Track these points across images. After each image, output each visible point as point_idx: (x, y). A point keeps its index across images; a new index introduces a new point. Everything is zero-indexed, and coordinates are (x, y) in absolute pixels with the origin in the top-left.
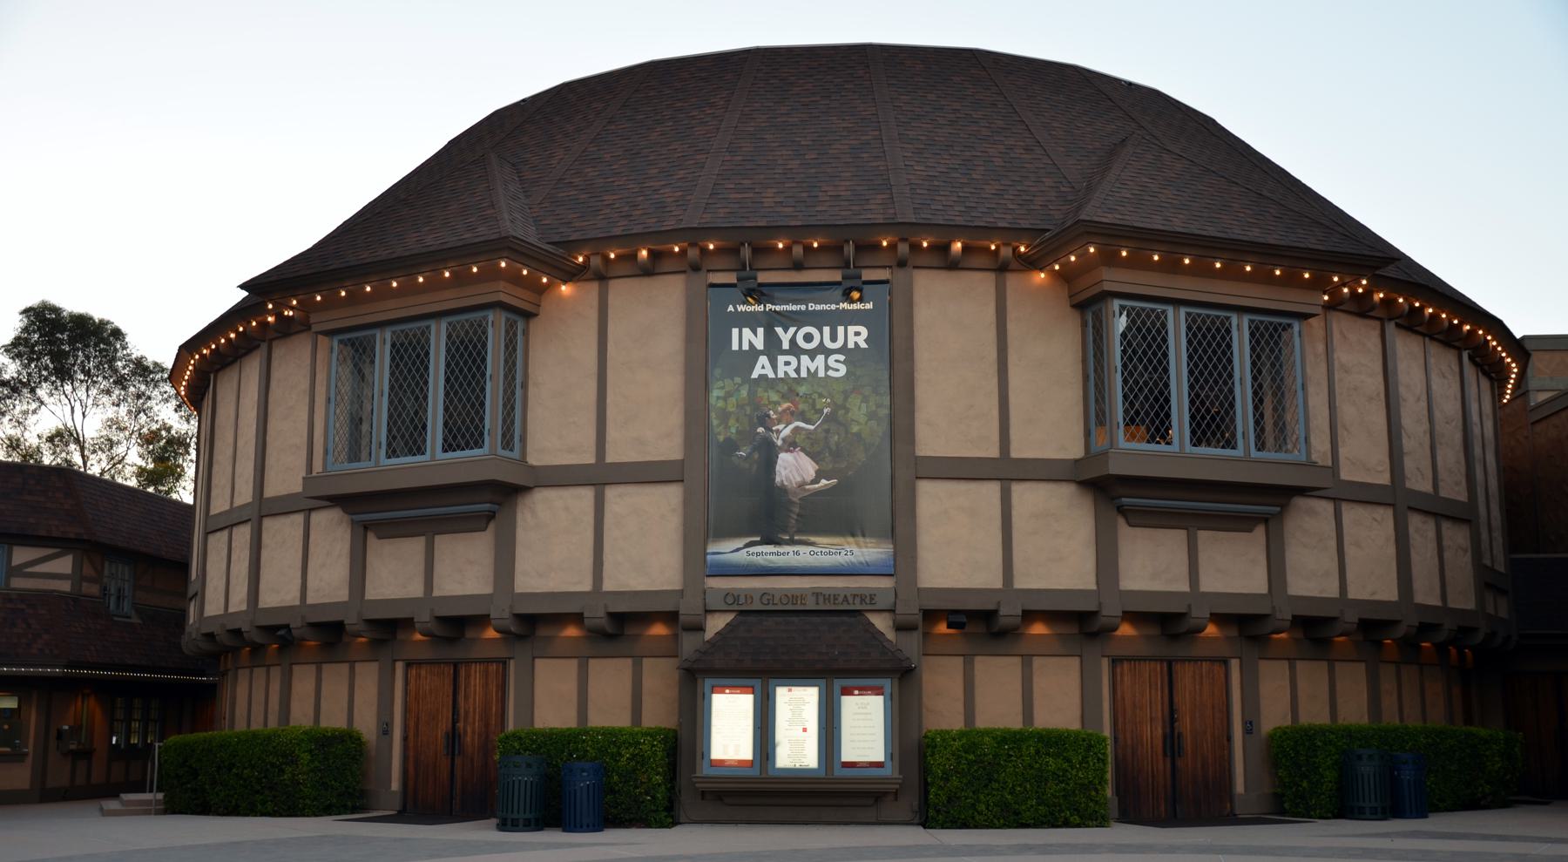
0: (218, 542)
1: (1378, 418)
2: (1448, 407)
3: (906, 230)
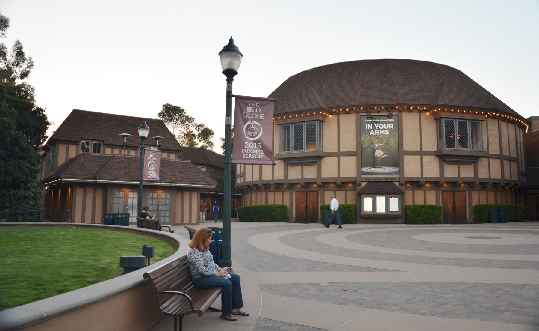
1: (497, 140)
2: (513, 137)
3: (401, 105)
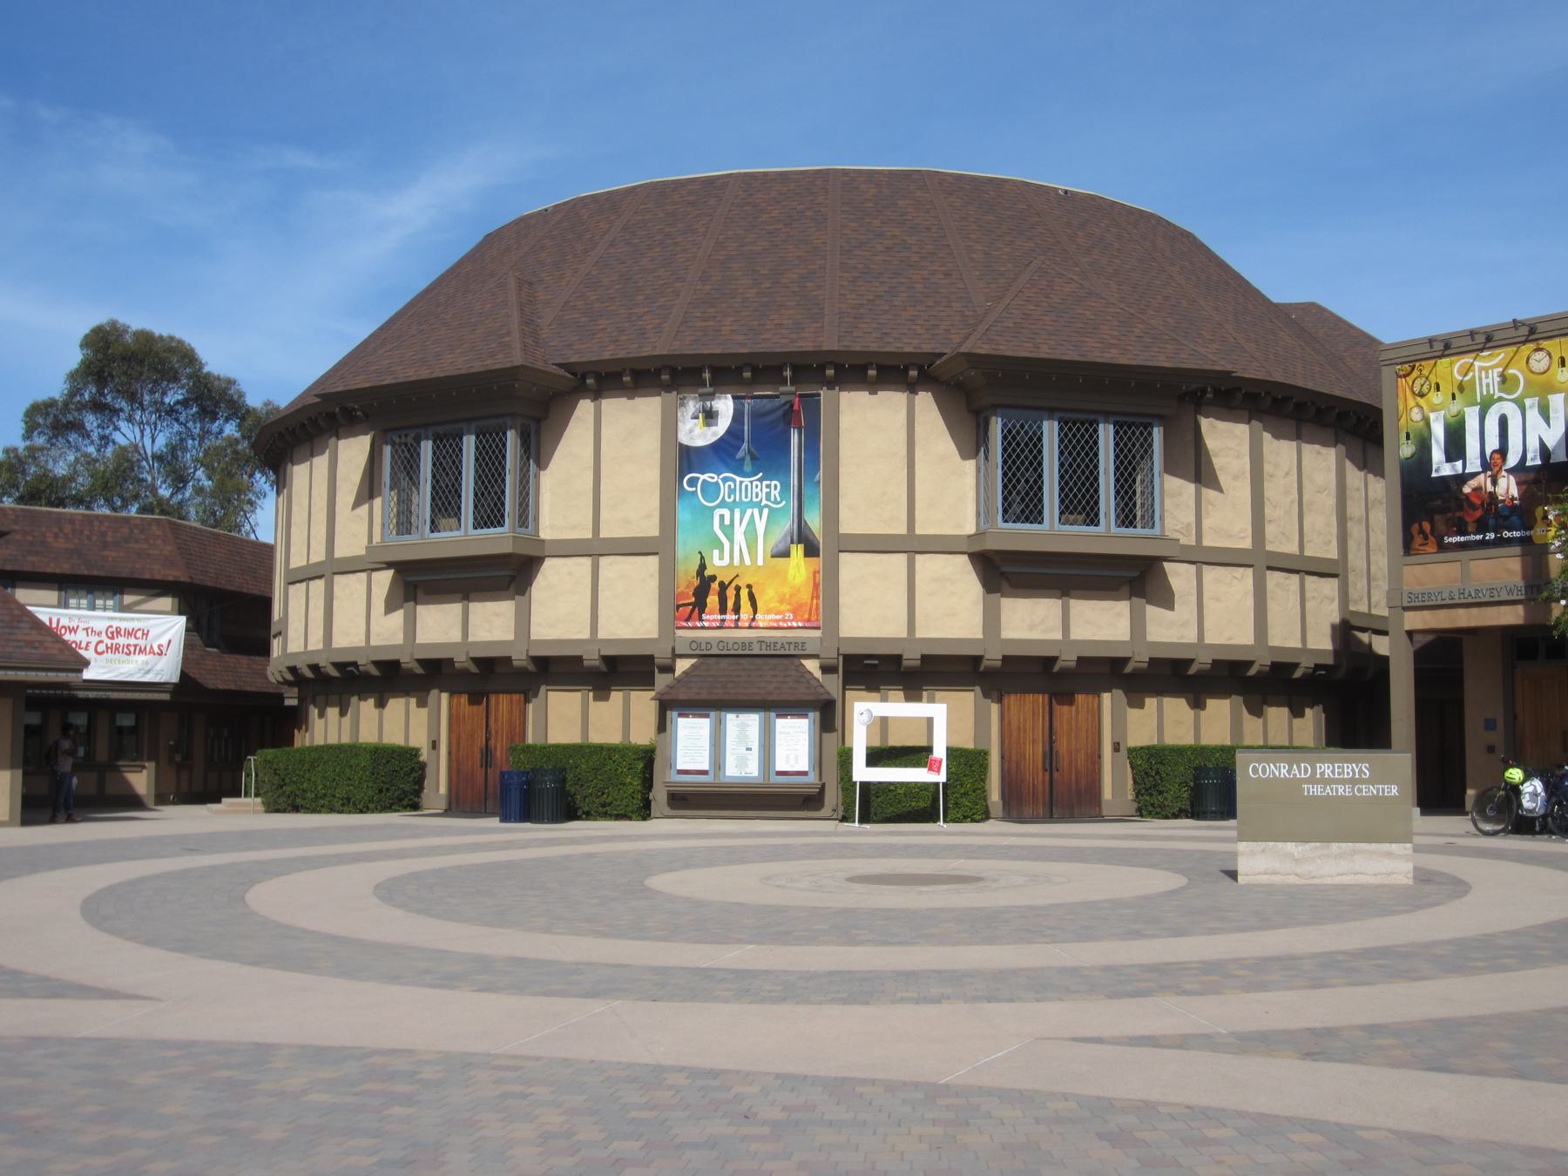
0: (297, 591)
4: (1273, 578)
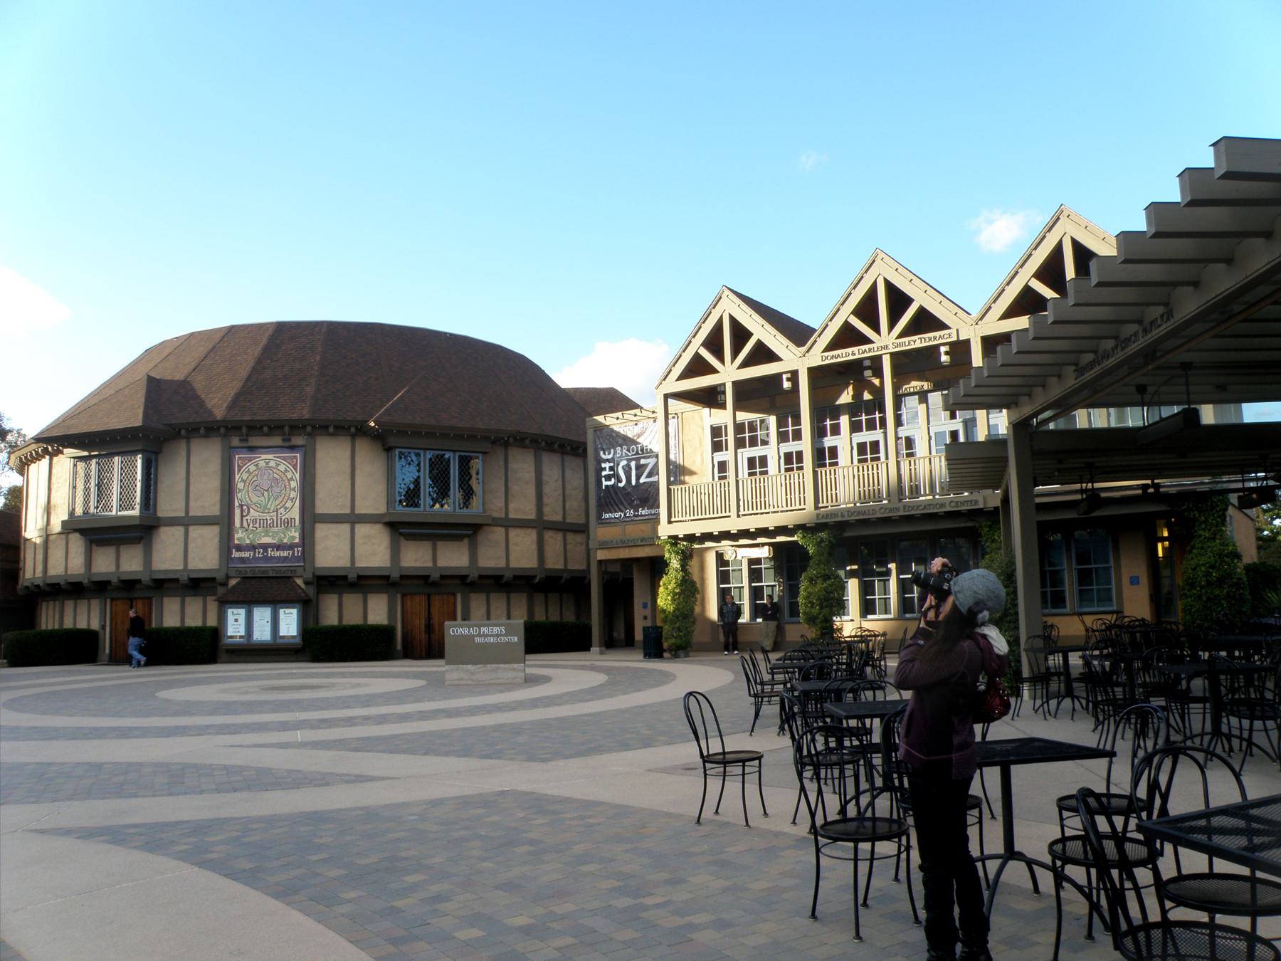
4: (548, 535)
